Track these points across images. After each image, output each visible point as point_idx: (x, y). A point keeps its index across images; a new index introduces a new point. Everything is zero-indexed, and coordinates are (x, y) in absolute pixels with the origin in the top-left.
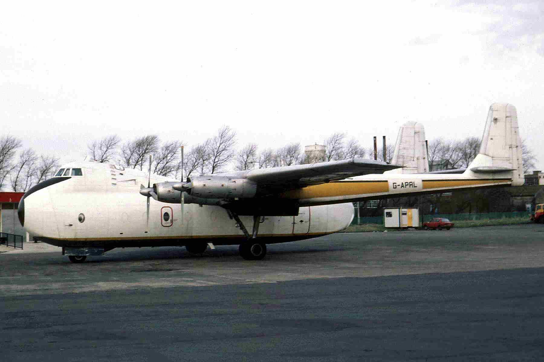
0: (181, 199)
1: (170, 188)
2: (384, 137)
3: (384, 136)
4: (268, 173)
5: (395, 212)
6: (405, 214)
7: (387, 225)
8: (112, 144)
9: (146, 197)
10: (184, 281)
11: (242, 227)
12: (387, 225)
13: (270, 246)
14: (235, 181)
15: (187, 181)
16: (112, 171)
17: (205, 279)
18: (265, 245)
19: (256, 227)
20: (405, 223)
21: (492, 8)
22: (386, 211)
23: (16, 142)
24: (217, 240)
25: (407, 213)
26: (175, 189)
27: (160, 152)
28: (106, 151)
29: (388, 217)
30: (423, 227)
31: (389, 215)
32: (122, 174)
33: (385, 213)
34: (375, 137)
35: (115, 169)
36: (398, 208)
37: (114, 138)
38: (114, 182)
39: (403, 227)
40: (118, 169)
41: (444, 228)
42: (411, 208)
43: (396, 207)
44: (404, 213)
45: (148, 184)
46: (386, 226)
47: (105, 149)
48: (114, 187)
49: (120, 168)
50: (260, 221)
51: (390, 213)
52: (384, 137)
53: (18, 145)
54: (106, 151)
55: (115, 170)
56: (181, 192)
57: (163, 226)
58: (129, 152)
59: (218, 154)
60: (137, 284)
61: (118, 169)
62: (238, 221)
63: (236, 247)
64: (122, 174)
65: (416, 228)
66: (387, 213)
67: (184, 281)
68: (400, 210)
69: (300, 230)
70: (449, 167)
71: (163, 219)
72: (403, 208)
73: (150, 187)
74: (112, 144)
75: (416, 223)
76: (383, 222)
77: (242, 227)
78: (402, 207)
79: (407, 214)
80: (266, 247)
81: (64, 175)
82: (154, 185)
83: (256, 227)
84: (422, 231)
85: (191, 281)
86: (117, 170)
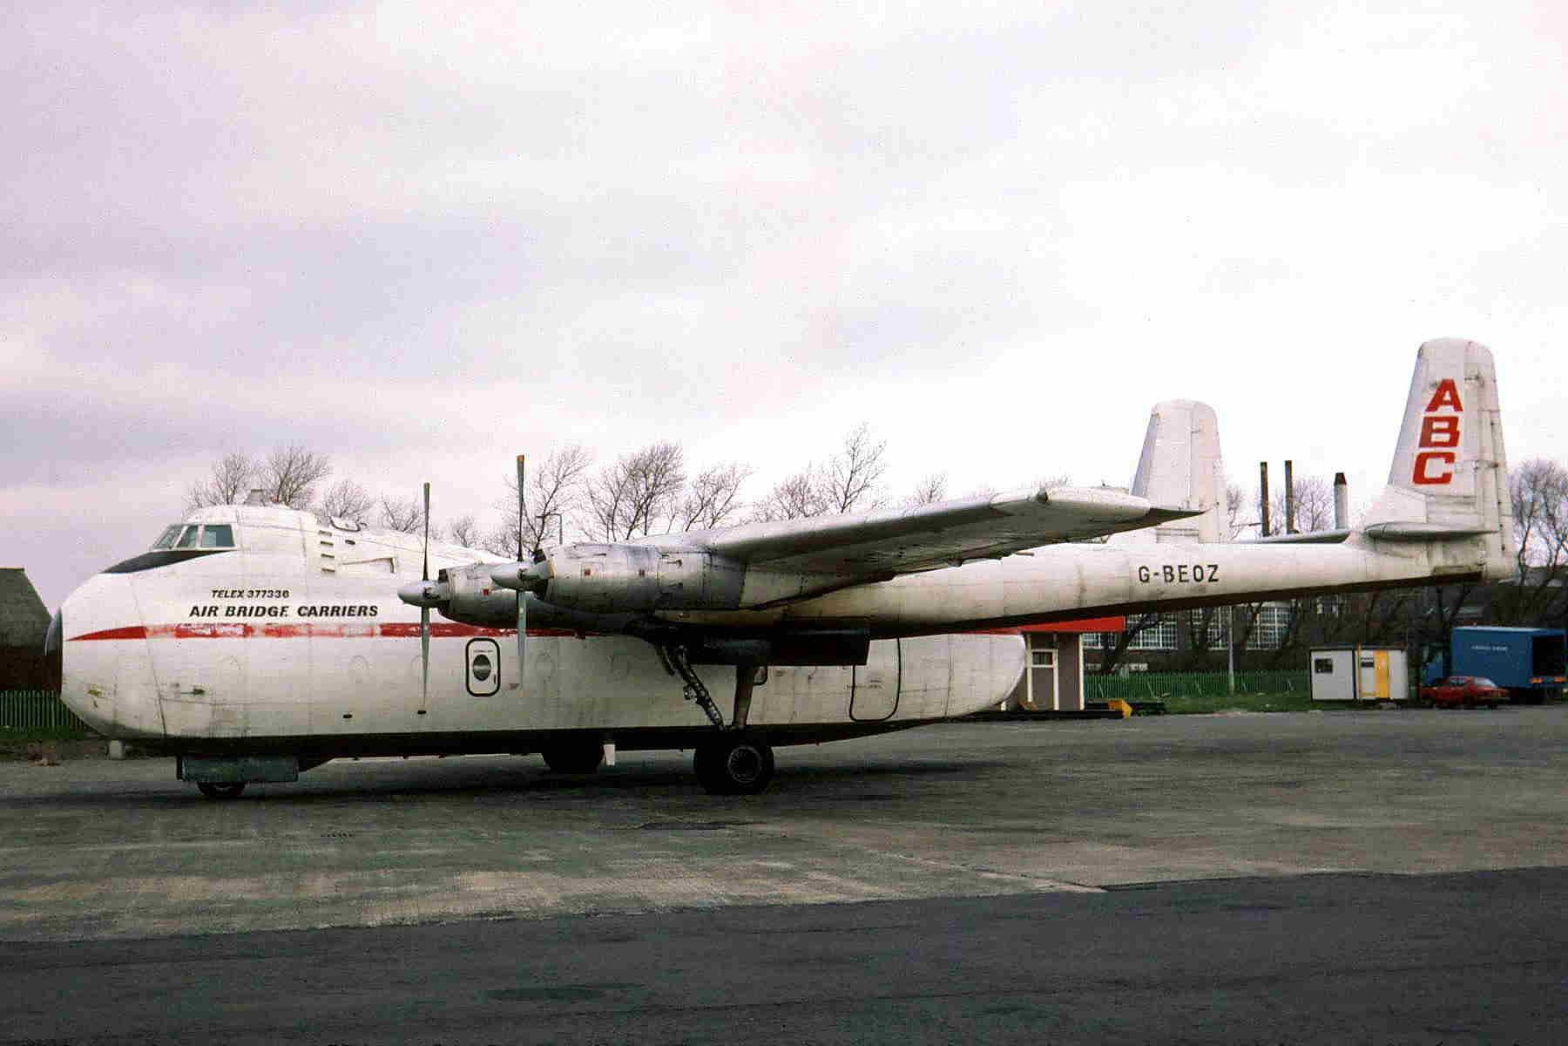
0: (518, 611)
1: (487, 583)
2: (1288, 464)
3: (1264, 461)
4: (739, 540)
5: (1341, 660)
6: (1371, 665)
7: (1318, 694)
8: (569, 471)
9: (419, 609)
10: (770, 873)
11: (704, 702)
12: (1318, 694)
13: (782, 754)
14: (680, 562)
15: (535, 559)
16: (323, 533)
17: (837, 864)
18: (770, 748)
19: (742, 697)
20: (1370, 687)
21: (163, 44)
22: (1315, 656)
23: (313, 463)
24: (628, 738)
25: (1376, 660)
26: (500, 583)
27: (687, 494)
28: (554, 492)
29: (1322, 671)
30: (1422, 696)
31: (1325, 667)
32: (352, 543)
33: (1050, 651)
34: (1264, 465)
35: (331, 526)
36: (1346, 649)
37: (573, 456)
38: (328, 565)
39: (1364, 701)
40: (341, 529)
41: (1482, 703)
42: (1387, 649)
43: (1344, 647)
44: (1365, 661)
45: (423, 570)
46: (1315, 697)
47: (550, 486)
48: (328, 578)
49: (347, 525)
50: (755, 681)
51: (1326, 660)
52: (1288, 464)
53: (321, 471)
54: (554, 492)
55: (330, 529)
56: (518, 591)
57: (471, 693)
58: (610, 495)
59: (848, 501)
60: (589, 886)
61: (341, 529)
62: (692, 684)
63: (537, 758)
64: (352, 543)
65: (1400, 704)
66: (1318, 661)
67: (770, 873)
68: (1356, 653)
69: (873, 707)
70: (810, 509)
71: (471, 675)
72: (1363, 649)
73: (430, 577)
74: (569, 471)
75: (1398, 687)
76: (1308, 687)
77: (704, 702)
78: (1362, 645)
79: (1376, 665)
80: (771, 754)
81: (178, 546)
82: (442, 572)
83: (742, 697)
84: (1413, 712)
85: (788, 876)
86: (337, 531)
